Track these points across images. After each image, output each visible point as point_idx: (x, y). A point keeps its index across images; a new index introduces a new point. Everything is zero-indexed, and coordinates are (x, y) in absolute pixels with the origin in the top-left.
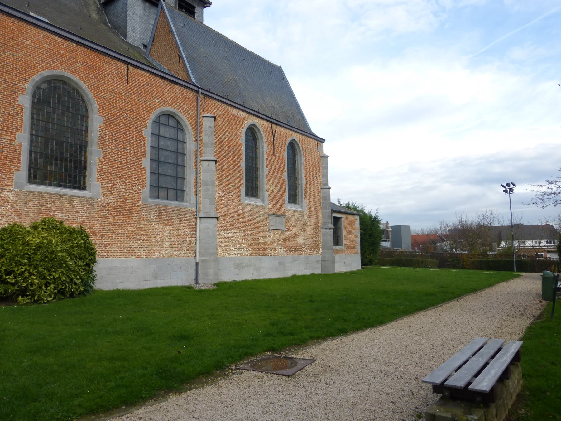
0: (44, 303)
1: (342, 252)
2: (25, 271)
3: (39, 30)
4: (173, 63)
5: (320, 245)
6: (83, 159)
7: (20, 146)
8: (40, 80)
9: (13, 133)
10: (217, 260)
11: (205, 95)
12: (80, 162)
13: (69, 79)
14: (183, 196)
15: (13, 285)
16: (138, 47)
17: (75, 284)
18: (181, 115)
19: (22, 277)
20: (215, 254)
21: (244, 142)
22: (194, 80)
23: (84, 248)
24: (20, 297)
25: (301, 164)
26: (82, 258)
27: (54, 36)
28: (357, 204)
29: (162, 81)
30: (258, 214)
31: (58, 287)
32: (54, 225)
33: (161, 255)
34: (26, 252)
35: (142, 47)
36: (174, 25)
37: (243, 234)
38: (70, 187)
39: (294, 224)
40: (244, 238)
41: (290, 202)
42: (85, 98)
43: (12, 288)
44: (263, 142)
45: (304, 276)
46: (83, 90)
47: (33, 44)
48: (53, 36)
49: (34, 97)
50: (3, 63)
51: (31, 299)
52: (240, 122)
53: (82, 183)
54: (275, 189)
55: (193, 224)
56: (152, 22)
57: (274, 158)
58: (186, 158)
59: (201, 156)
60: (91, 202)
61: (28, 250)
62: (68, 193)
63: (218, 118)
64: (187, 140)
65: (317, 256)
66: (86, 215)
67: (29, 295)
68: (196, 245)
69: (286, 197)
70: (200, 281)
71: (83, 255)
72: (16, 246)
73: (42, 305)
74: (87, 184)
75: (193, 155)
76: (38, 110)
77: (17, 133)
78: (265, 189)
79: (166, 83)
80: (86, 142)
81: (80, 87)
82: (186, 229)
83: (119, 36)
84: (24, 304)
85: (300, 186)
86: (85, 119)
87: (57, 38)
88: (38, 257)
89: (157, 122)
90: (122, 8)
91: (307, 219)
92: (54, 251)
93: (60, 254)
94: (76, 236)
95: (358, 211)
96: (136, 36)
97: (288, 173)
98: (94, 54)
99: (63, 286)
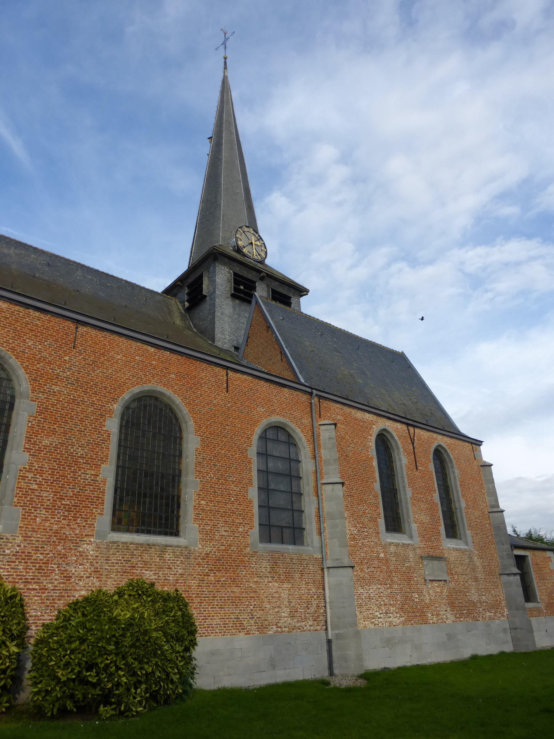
0: (133, 716)
1: (539, 612)
2: (111, 663)
3: (131, 341)
4: (274, 363)
5: (503, 603)
6: (176, 493)
7: (104, 482)
8: (130, 398)
9: (98, 466)
10: (358, 634)
11: (320, 397)
12: (173, 497)
13: (161, 393)
14: (303, 536)
15: (94, 685)
16: (228, 350)
17: (172, 682)
18: (293, 425)
19: (106, 673)
20: (355, 624)
21: (375, 454)
22: (302, 380)
23: (183, 622)
24: (102, 706)
25: (455, 479)
26: (179, 639)
27: (147, 346)
28: (542, 533)
29: (267, 385)
30: (406, 559)
31: (151, 688)
32: (144, 590)
33: (279, 629)
34: (113, 633)
35: (233, 349)
36: (272, 318)
37: (389, 591)
38: (160, 533)
39: (459, 570)
40: (391, 596)
41: (448, 536)
42: (179, 415)
43: (93, 692)
44: (399, 452)
45: (490, 657)
46: (177, 405)
47: (124, 358)
48: (146, 347)
49: (122, 419)
50: (92, 383)
51: (114, 709)
52: (366, 428)
53: (175, 527)
54: (425, 518)
55: (319, 577)
56: (244, 320)
57: (417, 473)
58: (303, 482)
59: (322, 478)
60: (186, 553)
61: (116, 630)
62: (159, 542)
63: (338, 425)
64: (302, 457)
65: (501, 622)
66: (180, 571)
67: (114, 703)
68: (325, 612)
69: (442, 529)
70: (336, 671)
71: (181, 634)
72: (101, 624)
73: (130, 719)
74: (181, 528)
75: (312, 478)
76: (126, 435)
77: (102, 465)
78: (412, 519)
79: (272, 386)
80: (180, 471)
81: (173, 402)
82: (311, 586)
83: (206, 341)
84: (107, 719)
85: (458, 511)
86: (178, 441)
87: (149, 348)
88: (128, 641)
89: (263, 437)
90: (210, 310)
91: (478, 562)
92: (147, 630)
93: (155, 634)
94: (171, 605)
95: (546, 543)
96: (226, 338)
97: (439, 493)
98: (188, 361)
99: (157, 685)
